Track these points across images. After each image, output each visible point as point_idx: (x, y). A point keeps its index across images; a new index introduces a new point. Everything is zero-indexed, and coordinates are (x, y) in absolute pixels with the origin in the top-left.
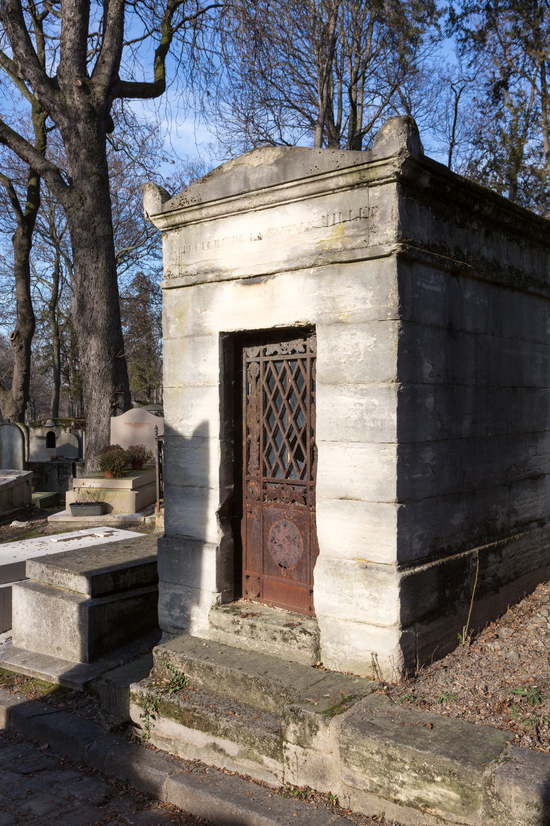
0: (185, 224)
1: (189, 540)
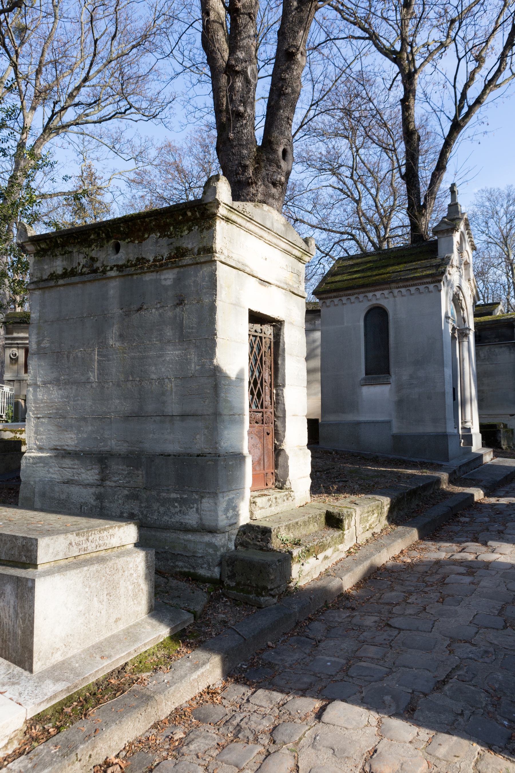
0: (233, 222)
1: (234, 455)
